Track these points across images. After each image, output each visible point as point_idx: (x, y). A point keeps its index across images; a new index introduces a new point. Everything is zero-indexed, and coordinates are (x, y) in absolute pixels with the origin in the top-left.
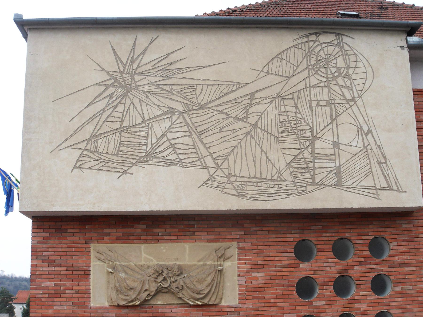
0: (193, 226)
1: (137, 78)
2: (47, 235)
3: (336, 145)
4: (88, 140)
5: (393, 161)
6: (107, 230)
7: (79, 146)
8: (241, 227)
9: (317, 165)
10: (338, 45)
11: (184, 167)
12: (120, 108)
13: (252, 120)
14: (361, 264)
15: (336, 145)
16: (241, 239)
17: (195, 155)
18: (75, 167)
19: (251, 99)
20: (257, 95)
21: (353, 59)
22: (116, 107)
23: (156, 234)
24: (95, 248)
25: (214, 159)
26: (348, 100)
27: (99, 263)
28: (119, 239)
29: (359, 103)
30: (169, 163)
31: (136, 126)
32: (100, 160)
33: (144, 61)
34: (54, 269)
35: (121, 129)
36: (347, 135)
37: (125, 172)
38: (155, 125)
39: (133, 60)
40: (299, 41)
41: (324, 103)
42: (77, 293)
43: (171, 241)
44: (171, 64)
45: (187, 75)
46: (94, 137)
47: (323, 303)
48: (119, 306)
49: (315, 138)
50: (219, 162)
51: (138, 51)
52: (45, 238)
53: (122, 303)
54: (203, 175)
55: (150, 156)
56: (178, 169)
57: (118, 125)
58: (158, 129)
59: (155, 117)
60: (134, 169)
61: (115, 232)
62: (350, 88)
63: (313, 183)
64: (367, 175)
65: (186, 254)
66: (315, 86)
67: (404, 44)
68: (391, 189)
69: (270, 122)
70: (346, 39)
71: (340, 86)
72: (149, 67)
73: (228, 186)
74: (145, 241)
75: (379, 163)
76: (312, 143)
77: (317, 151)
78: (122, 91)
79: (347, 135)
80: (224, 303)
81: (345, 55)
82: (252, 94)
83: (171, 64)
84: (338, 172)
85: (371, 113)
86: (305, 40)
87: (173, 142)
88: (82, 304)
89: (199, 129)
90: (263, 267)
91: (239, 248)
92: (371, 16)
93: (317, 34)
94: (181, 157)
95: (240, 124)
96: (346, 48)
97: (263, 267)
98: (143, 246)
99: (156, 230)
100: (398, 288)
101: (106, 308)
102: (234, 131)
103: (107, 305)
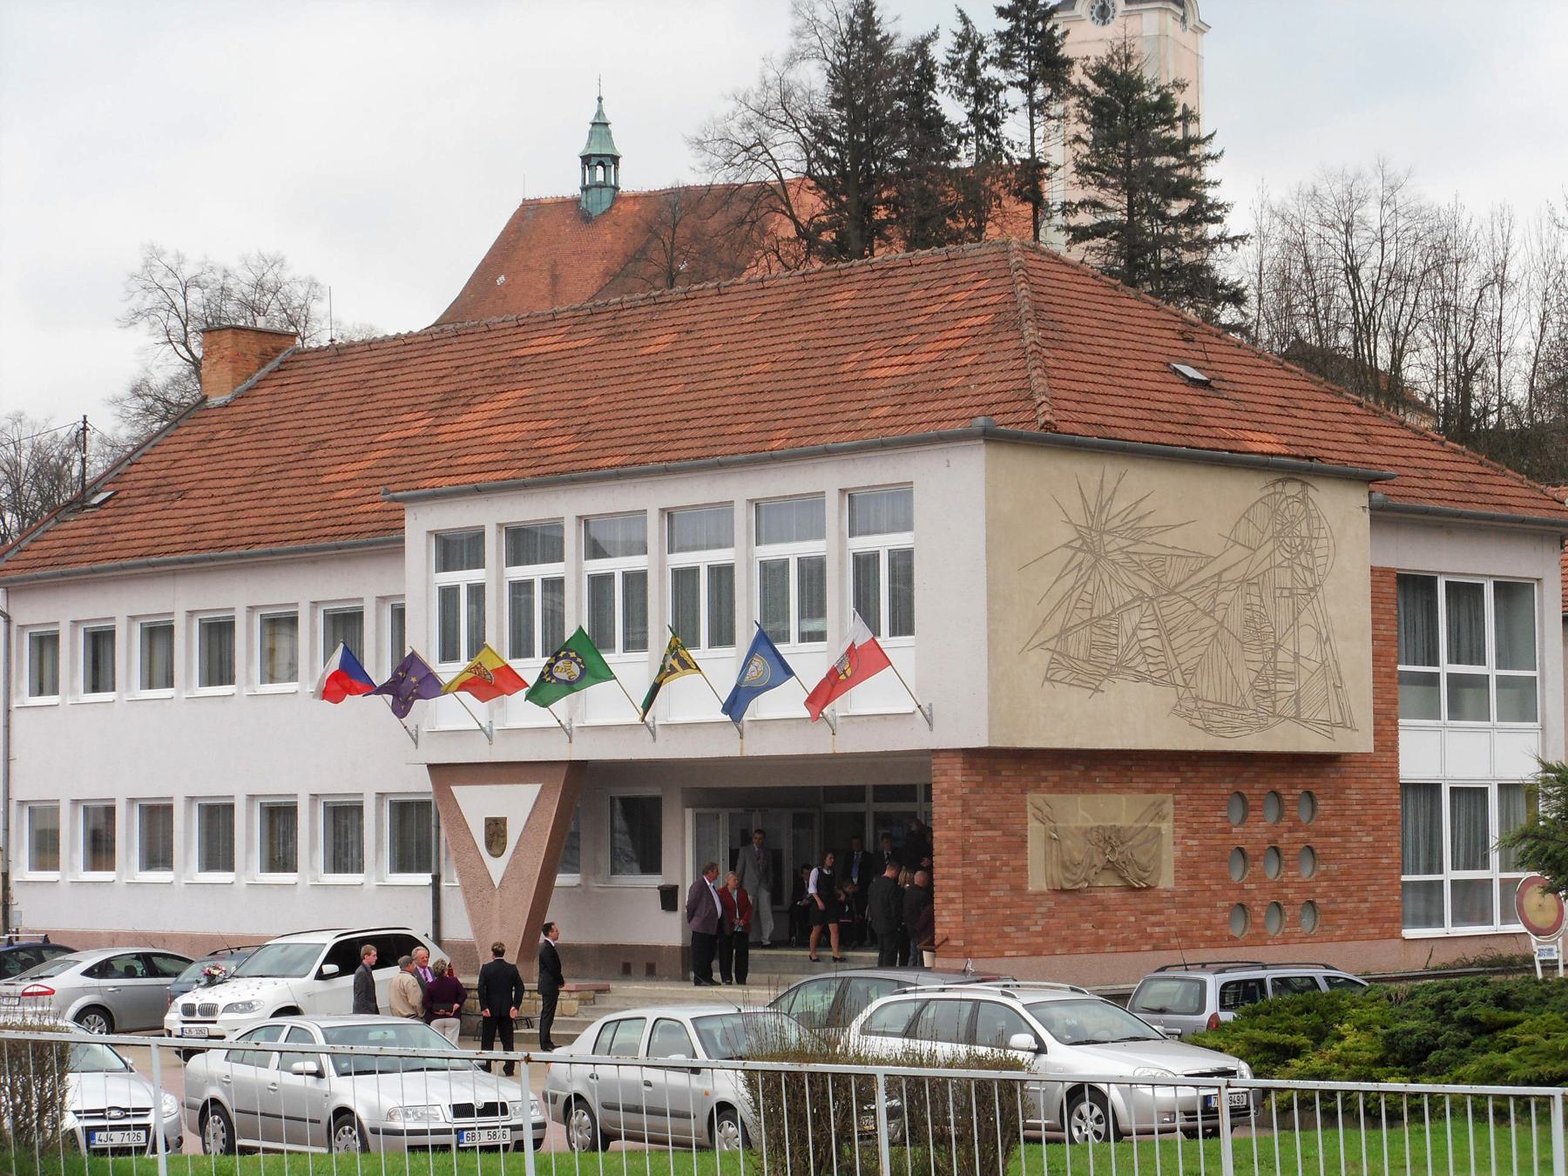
0: (1128, 768)
1: (1107, 538)
2: (979, 779)
3: (1296, 656)
4: (1058, 636)
5: (1348, 685)
6: (1044, 773)
7: (1048, 645)
8: (1175, 770)
9: (1279, 687)
10: (1302, 502)
11: (1154, 683)
12: (1089, 588)
13: (1219, 615)
14: (1290, 830)
15: (1296, 656)
16: (1176, 791)
17: (1163, 666)
18: (1047, 679)
19: (1219, 582)
20: (1226, 576)
21: (1316, 524)
22: (1085, 584)
23: (1092, 780)
24: (1034, 799)
25: (1183, 673)
26: (1311, 590)
27: (1037, 824)
28: (1058, 787)
29: (1320, 594)
30: (1140, 678)
31: (1106, 616)
32: (1071, 669)
33: (1114, 511)
34: (989, 833)
35: (1091, 622)
36: (1307, 646)
37: (1097, 690)
38: (1125, 616)
39: (1102, 509)
40: (1266, 492)
41: (1286, 593)
42: (1014, 870)
43: (1110, 791)
44: (1140, 518)
45: (1155, 539)
46: (1065, 631)
47: (1253, 886)
48: (1063, 891)
49: (1278, 646)
50: (1187, 677)
51: (1107, 494)
52: (979, 785)
53: (1067, 886)
54: (1170, 696)
55: (1120, 668)
56: (1148, 686)
57: (1086, 616)
58: (1131, 619)
59: (1126, 604)
60: (1105, 685)
61: (1053, 775)
62: (1311, 571)
63: (1274, 714)
64: (1323, 705)
65: (1119, 808)
66: (1279, 566)
67: (1365, 502)
68: (1345, 727)
69: (1235, 620)
70: (1311, 492)
71: (1304, 567)
72: (1117, 522)
73: (1196, 715)
74: (1083, 791)
75: (1336, 687)
76: (1275, 655)
77: (1279, 666)
78: (1090, 559)
79: (1307, 646)
80: (1161, 886)
81: (1309, 517)
82: (1220, 574)
83: (1140, 518)
84: (1297, 698)
85: (1332, 610)
86: (1272, 490)
87: (1143, 644)
88: (1018, 889)
89: (1169, 626)
90: (1197, 831)
91: (1176, 803)
92: (881, 278)
93: (1284, 481)
94: (1152, 668)
95: (1207, 621)
96: (1311, 507)
97: (1197, 831)
98: (1080, 798)
99: (1094, 774)
100: (1323, 868)
101: (1042, 894)
102: (1202, 631)
103: (1045, 889)
